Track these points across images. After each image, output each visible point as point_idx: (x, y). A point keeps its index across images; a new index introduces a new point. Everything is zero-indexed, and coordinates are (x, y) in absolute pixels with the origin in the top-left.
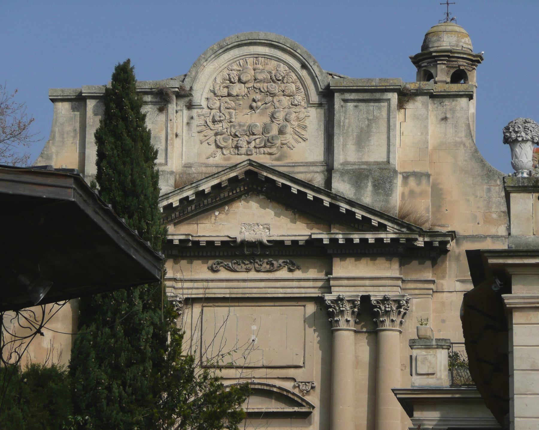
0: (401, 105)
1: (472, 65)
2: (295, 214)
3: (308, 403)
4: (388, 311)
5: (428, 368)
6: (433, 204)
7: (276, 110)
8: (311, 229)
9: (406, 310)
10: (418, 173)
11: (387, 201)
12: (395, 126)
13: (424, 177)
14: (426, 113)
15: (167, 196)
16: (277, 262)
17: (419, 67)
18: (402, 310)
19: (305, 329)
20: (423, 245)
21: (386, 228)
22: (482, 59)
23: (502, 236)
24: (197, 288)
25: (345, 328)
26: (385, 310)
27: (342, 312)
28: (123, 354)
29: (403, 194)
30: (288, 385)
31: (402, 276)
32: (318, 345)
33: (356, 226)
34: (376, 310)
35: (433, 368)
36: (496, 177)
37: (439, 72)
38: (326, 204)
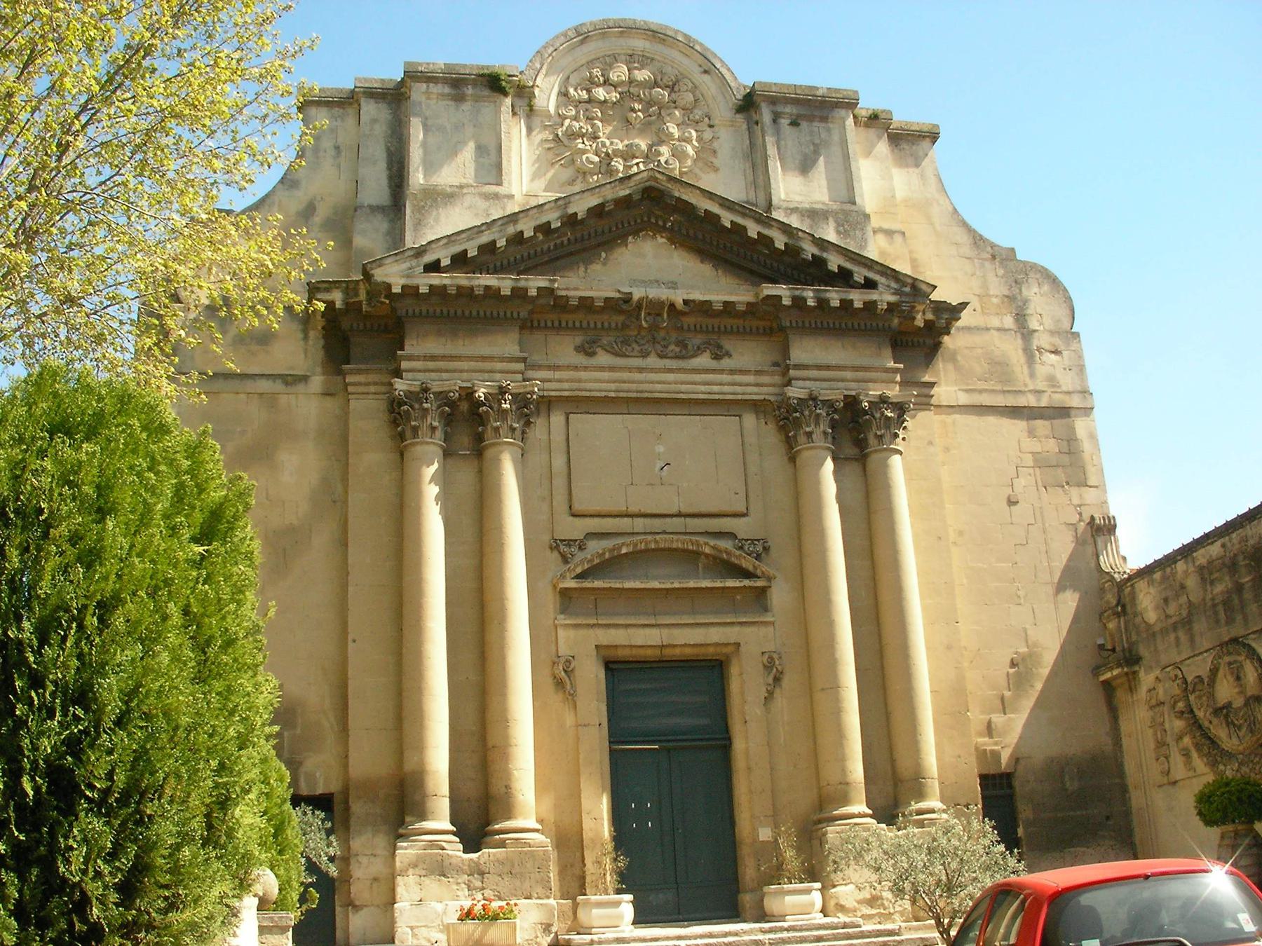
24: (560, 381)
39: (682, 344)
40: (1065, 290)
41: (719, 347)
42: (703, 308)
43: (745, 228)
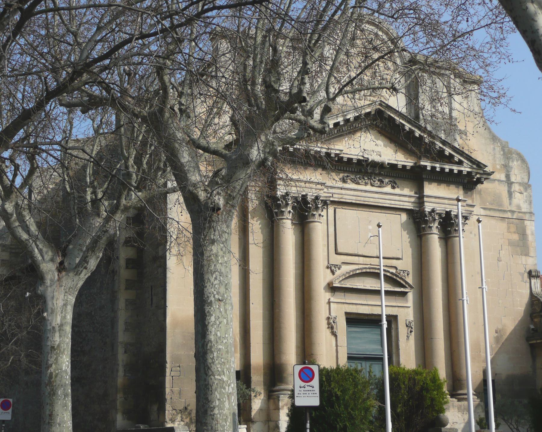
2: (396, 147)
8: (407, 159)
23: (503, 181)
39: (382, 182)
40: (527, 164)
41: (395, 183)
42: (393, 167)
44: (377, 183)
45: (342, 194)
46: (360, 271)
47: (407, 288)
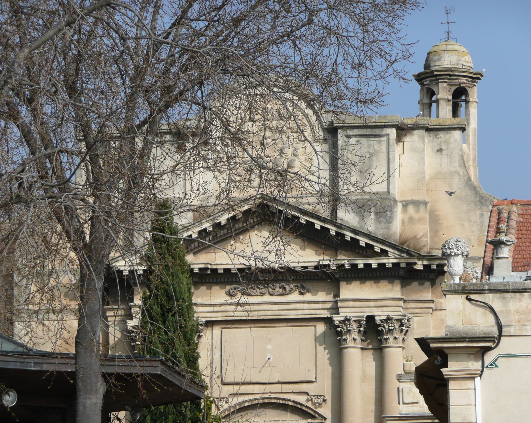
0: (399, 139)
1: (473, 82)
2: (304, 242)
3: (320, 415)
4: (391, 330)
5: (413, 398)
6: (431, 229)
7: (285, 146)
8: (319, 255)
9: (408, 327)
10: (416, 201)
11: (388, 229)
12: (394, 159)
13: (422, 205)
14: (423, 145)
15: (186, 228)
16: (289, 286)
17: (422, 84)
18: (404, 328)
19: (316, 347)
20: (422, 268)
21: (388, 254)
22: (482, 76)
25: (352, 345)
26: (389, 329)
27: (349, 331)
28: (170, 417)
29: (403, 222)
30: (302, 399)
31: (403, 297)
32: (329, 362)
33: (361, 252)
34: (380, 328)
35: (417, 398)
36: (488, 203)
37: (440, 90)
38: (333, 233)
43: (313, 224)
44: (279, 290)
45: (227, 312)
46: (250, 403)
47: (316, 418)
